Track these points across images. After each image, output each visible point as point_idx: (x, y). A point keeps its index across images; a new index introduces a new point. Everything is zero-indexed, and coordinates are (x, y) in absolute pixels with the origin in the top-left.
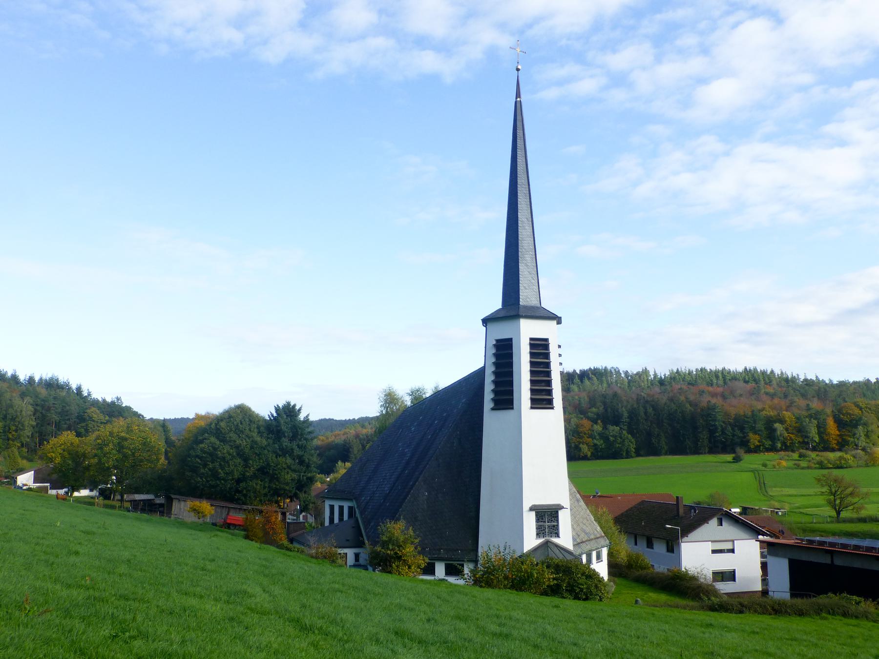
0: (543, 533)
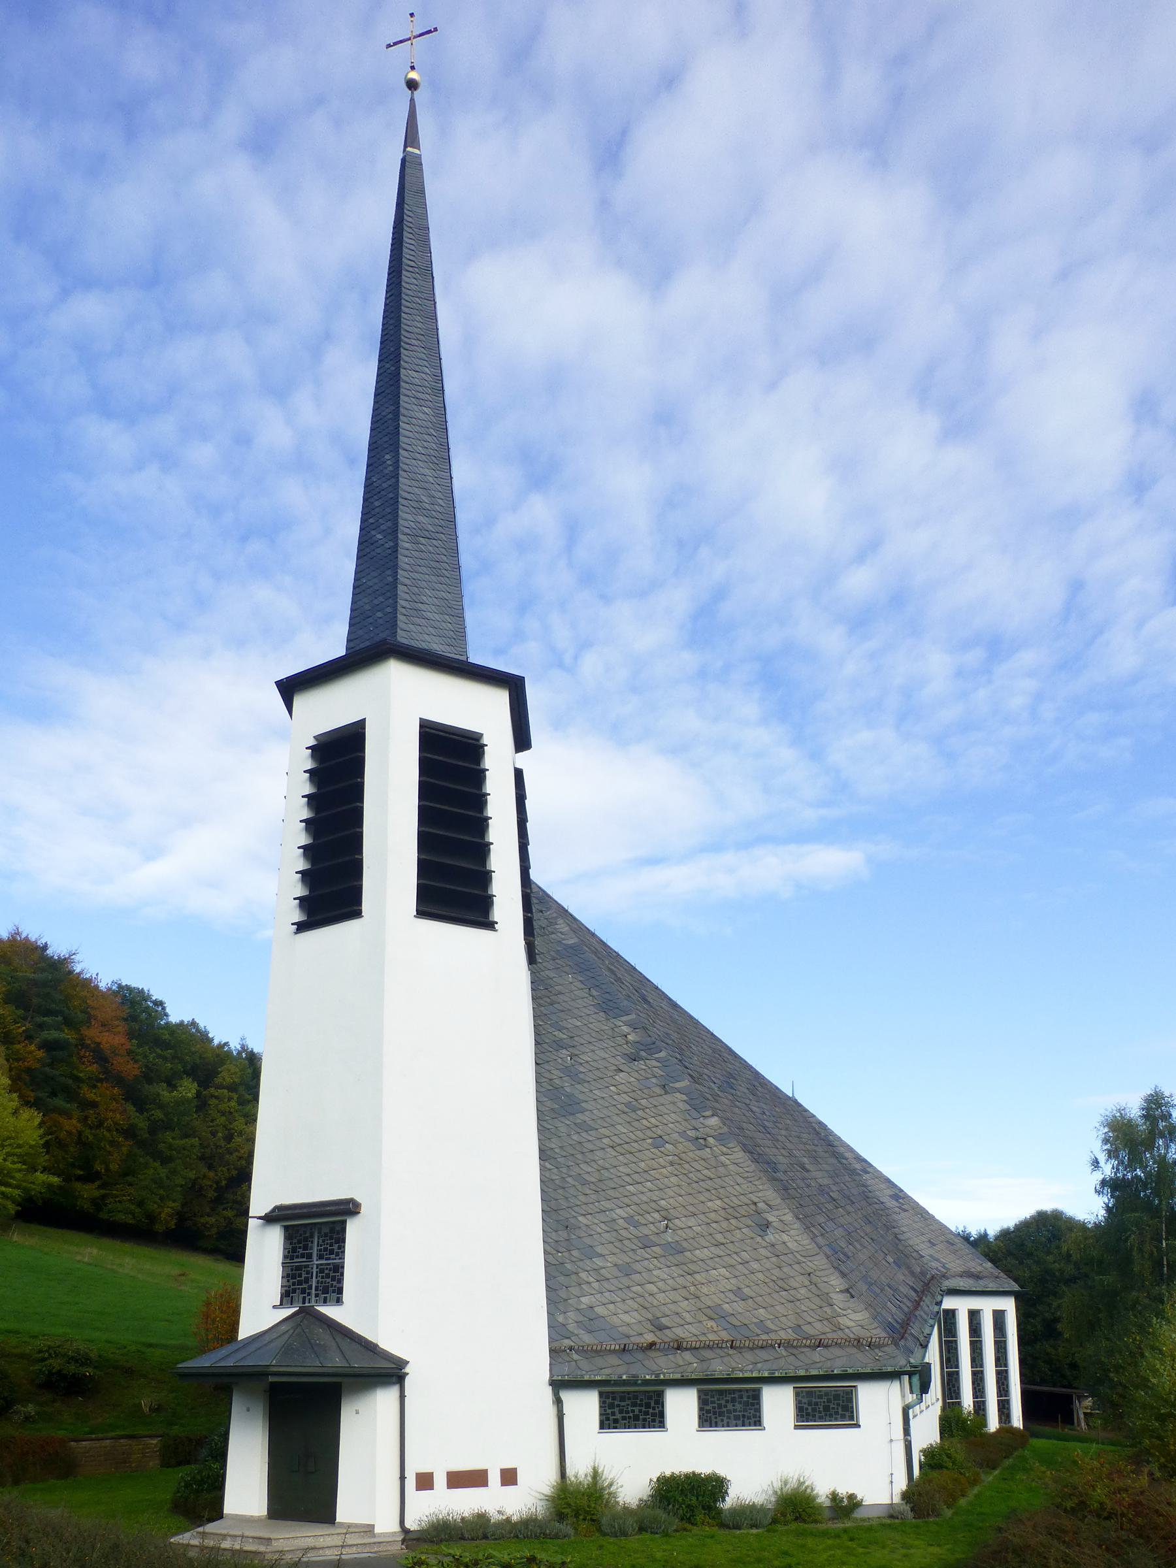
0: (303, 1291)
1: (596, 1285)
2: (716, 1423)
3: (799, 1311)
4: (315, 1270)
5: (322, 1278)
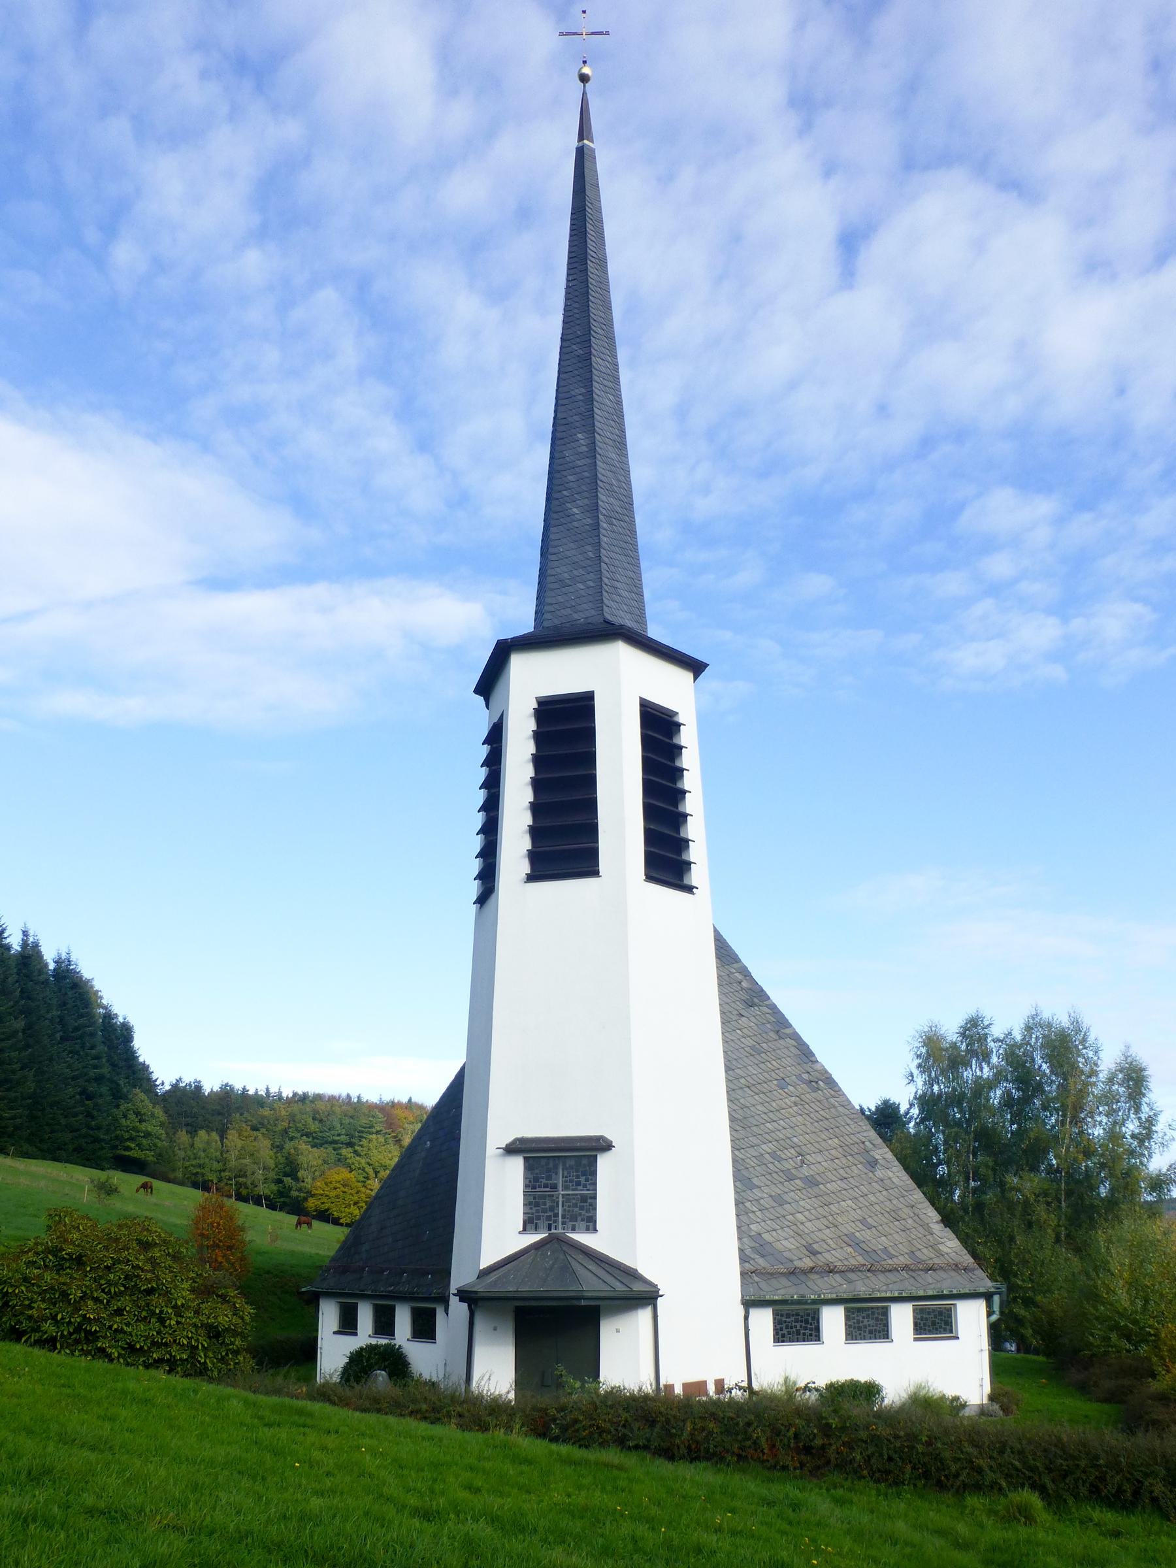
0: (549, 1218)
1: (759, 1213)
2: (856, 1336)
3: (910, 1239)
4: (561, 1200)
5: (569, 1206)
